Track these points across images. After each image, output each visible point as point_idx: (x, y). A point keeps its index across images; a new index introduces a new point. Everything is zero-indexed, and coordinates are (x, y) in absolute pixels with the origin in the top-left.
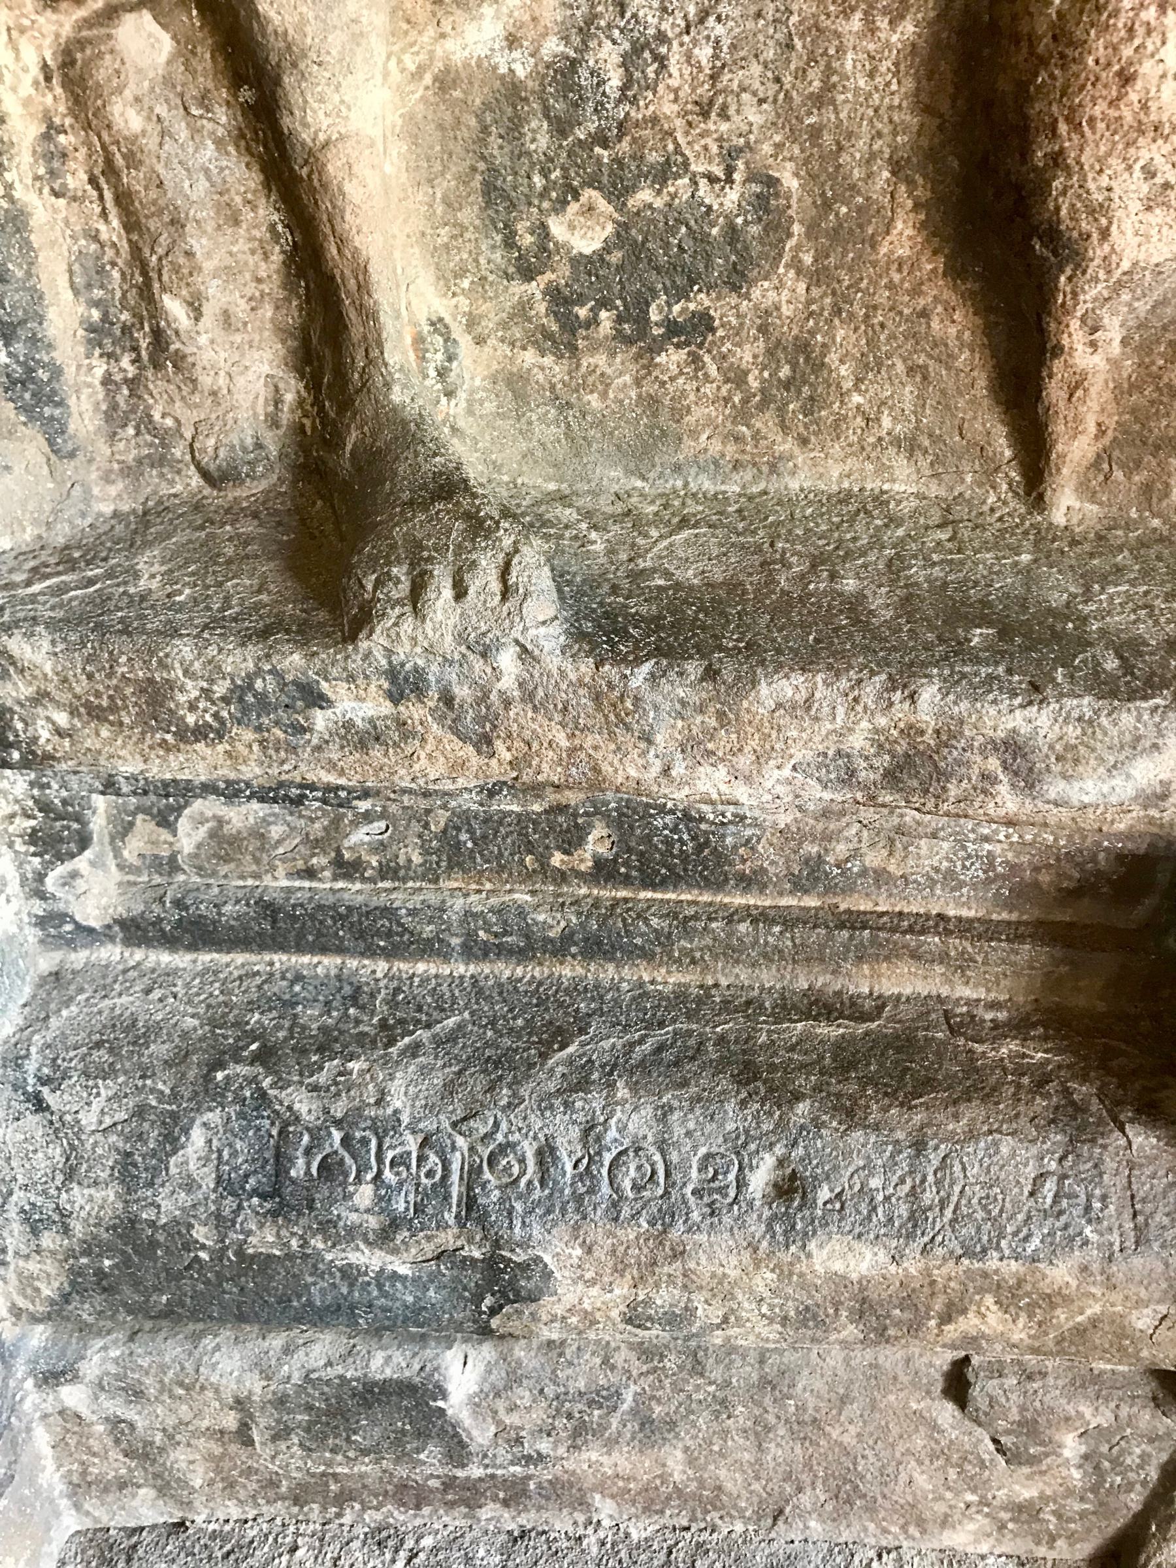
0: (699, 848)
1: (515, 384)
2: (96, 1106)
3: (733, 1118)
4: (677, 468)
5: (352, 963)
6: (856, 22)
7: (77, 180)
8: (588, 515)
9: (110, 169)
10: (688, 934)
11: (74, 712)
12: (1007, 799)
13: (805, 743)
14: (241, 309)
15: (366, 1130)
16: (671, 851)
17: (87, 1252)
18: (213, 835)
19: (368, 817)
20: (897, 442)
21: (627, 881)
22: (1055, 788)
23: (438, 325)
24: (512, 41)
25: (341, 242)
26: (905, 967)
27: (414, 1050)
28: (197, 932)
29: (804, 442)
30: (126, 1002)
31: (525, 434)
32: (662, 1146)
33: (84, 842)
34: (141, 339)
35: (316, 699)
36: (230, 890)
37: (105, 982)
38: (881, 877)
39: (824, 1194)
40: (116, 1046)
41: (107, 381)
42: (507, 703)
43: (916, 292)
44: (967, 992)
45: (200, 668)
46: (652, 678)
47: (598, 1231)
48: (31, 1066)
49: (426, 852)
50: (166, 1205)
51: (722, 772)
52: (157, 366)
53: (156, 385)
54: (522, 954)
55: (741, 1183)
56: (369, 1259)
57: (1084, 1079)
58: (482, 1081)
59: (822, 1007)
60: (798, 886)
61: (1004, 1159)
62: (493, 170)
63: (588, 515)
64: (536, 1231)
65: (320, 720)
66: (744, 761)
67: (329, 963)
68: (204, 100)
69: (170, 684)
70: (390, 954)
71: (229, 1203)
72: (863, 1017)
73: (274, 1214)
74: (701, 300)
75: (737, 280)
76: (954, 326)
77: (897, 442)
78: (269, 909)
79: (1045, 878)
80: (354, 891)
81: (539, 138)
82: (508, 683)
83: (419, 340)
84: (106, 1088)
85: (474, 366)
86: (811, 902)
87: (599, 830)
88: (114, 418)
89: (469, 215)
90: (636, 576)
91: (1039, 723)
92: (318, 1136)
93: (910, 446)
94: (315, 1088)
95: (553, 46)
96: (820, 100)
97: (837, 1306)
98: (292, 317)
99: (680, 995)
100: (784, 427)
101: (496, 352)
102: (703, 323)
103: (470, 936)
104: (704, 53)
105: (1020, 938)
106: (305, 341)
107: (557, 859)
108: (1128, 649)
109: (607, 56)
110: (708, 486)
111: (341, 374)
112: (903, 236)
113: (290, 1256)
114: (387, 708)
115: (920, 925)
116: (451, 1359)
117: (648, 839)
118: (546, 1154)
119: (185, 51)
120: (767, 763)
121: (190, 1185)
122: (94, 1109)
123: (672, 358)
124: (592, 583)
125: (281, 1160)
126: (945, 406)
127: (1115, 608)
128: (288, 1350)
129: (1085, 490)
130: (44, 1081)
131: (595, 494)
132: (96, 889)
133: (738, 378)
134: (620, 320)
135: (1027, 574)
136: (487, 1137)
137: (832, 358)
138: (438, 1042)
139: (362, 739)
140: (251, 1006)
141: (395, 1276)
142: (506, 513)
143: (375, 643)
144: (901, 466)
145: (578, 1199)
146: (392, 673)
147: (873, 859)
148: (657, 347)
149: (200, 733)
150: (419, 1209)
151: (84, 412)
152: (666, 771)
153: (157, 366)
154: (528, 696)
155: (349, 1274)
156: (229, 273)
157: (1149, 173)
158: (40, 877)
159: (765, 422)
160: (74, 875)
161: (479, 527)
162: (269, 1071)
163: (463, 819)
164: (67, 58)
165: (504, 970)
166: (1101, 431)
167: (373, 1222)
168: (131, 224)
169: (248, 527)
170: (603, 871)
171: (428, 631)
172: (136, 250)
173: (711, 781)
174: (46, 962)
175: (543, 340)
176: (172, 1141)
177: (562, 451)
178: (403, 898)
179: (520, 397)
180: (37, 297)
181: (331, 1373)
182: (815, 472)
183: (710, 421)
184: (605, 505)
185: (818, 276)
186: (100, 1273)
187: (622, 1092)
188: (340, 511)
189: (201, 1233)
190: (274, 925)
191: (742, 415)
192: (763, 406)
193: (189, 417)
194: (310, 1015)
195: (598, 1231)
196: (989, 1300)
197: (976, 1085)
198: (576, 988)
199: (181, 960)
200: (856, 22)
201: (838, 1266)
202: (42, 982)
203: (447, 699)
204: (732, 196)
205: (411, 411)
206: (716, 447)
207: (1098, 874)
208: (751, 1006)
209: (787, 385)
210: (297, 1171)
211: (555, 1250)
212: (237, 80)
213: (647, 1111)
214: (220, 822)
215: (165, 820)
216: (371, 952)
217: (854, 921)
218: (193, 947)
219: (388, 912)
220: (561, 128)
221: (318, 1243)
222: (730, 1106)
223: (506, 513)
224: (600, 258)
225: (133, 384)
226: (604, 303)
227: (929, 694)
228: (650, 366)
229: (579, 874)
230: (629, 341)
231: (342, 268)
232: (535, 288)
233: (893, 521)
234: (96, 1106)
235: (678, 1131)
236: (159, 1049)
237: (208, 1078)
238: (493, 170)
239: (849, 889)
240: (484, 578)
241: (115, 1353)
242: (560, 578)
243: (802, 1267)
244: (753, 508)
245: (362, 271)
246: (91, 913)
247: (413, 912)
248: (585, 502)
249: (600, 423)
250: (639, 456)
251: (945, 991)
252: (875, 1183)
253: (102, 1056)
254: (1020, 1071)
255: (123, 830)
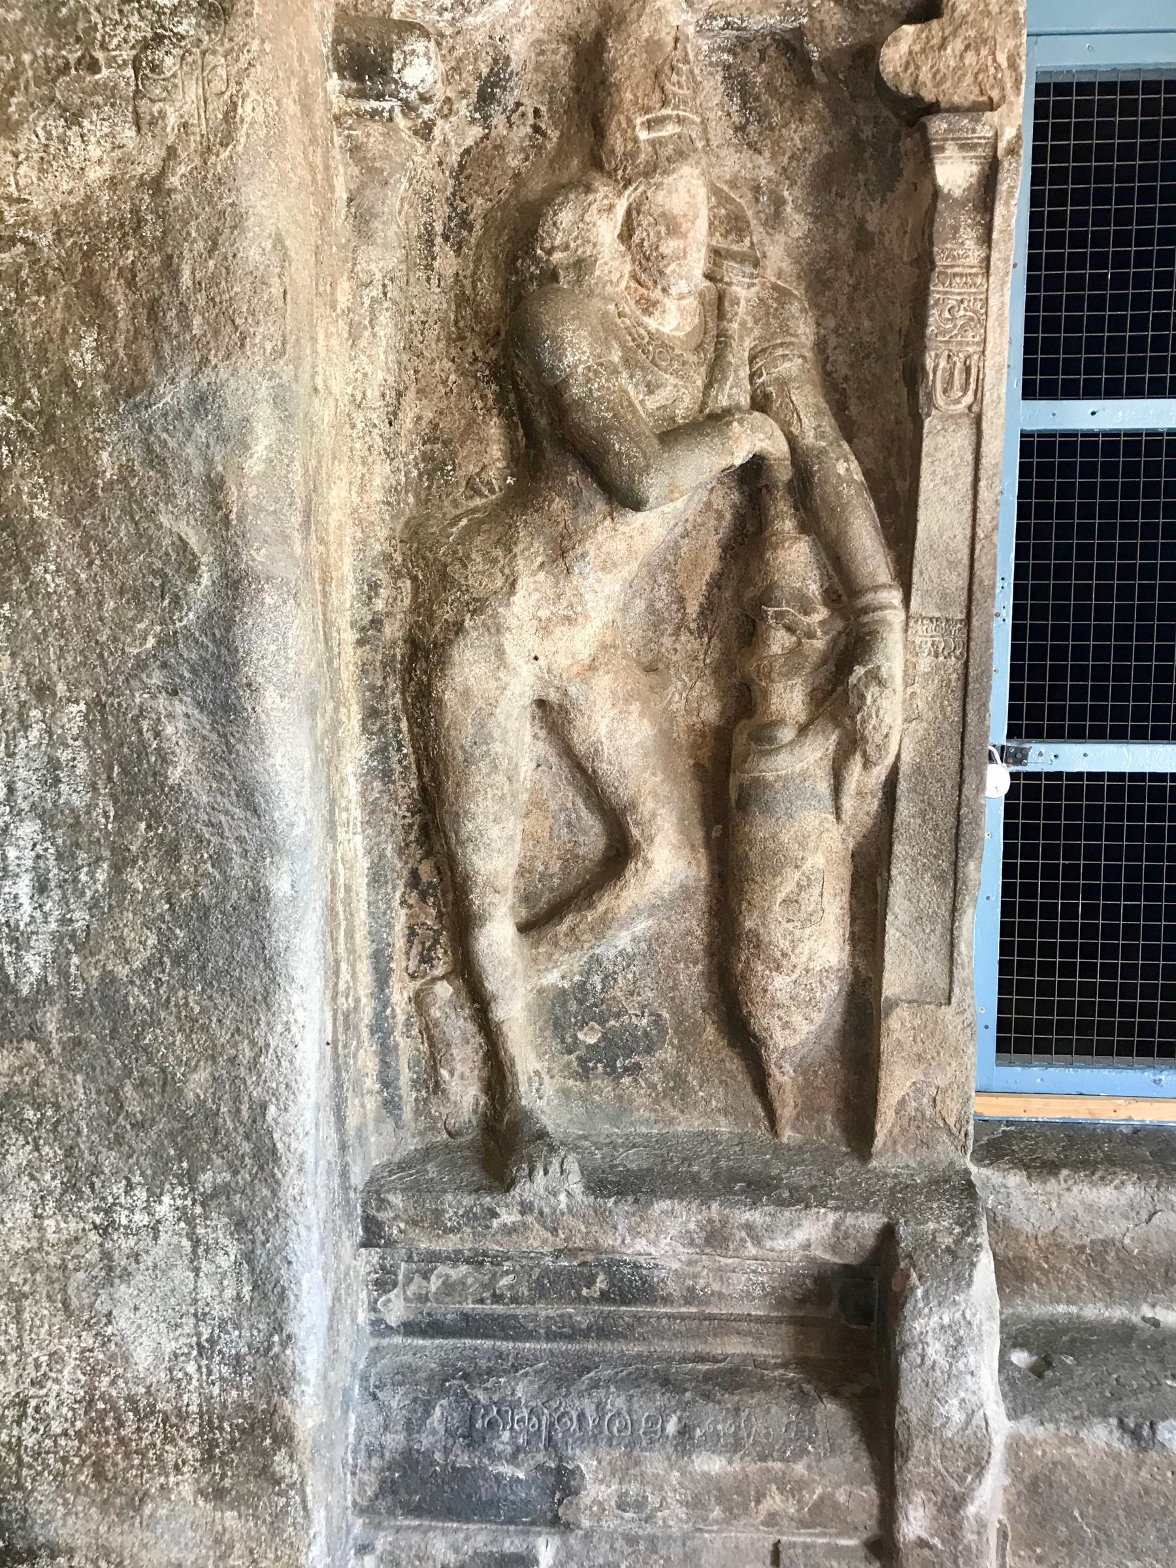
0: (644, 1283)
1: (566, 1093)
2: (398, 1397)
3: (660, 1400)
4: (632, 1123)
5: (498, 1343)
6: (682, 965)
7: (415, 1032)
8: (595, 1144)
9: (427, 1028)
10: (641, 1325)
11: (407, 1223)
12: (752, 1250)
13: (673, 1227)
14: (467, 1072)
15: (507, 1406)
16: (632, 1287)
17: (389, 1469)
18: (444, 1283)
19: (507, 1273)
20: (719, 1111)
21: (614, 1302)
22: (768, 1244)
23: (537, 1073)
24: (563, 978)
25: (506, 1051)
26: (735, 1339)
27: (526, 1374)
28: (433, 1328)
29: (682, 1112)
30: (407, 1358)
31: (570, 1112)
32: (629, 1413)
33: (395, 1285)
34: (431, 1082)
35: (495, 1215)
36: (449, 1311)
37: (397, 1351)
38: (720, 1295)
39: (698, 1432)
40: (404, 1375)
41: (416, 1099)
42: (563, 1214)
43: (718, 1053)
44: (764, 1352)
45: (454, 1204)
46: (615, 1203)
47: (602, 1452)
48: (372, 1381)
49: (530, 1290)
50: (424, 1442)
51: (644, 1241)
52: (435, 1093)
53: (434, 1100)
54: (570, 1338)
55: (663, 1429)
56: (506, 1470)
57: (809, 1382)
58: (554, 1386)
59: (700, 1358)
60: (687, 1303)
61: (772, 1416)
62: (557, 1018)
63: (595, 1144)
64: (578, 1452)
65: (495, 1223)
66: (652, 1236)
67: (488, 1343)
68: (462, 1007)
69: (444, 1211)
70: (515, 1339)
71: (450, 1441)
72: (718, 1362)
73: (468, 1445)
74: (636, 1058)
75: (649, 1051)
76: (734, 1064)
77: (719, 1111)
78: (465, 1316)
79: (788, 1294)
80: (499, 1309)
81: (573, 1006)
82: (563, 1206)
83: (530, 1078)
84: (401, 1390)
85: (549, 1087)
86: (694, 1310)
87: (601, 1278)
88: (417, 1112)
89: (547, 1034)
90: (612, 1167)
91: (755, 1216)
92: (487, 1410)
93: (725, 1112)
94: (486, 1389)
95: (577, 978)
96: (673, 989)
97: (709, 1492)
98: (485, 1074)
99: (639, 1355)
100: (674, 1107)
101: (559, 1080)
102: (637, 1066)
103: (549, 1328)
104: (630, 976)
105: (781, 1322)
106: (489, 1083)
107: (585, 1292)
108: (793, 1189)
109: (596, 980)
110: (644, 1130)
111: (503, 1095)
112: (710, 1032)
113: (474, 1468)
114: (519, 1218)
115: (739, 1319)
116: (541, 1542)
117: (621, 1280)
118: (581, 1416)
119: (457, 992)
120: (660, 1240)
121: (434, 1432)
122: (396, 1400)
123: (626, 1080)
124: (595, 1170)
125: (472, 1421)
126: (736, 1096)
127: (796, 1175)
128: (466, 1539)
129: (794, 1128)
130: (376, 1387)
131: (598, 1135)
132: (396, 1309)
133: (653, 1087)
134: (605, 1067)
135: (767, 1163)
136: (557, 1409)
137: (690, 1078)
138: (536, 1372)
139: (509, 1230)
140: (458, 1359)
141: (518, 1480)
142: (562, 1143)
143: (516, 1192)
144: (723, 1120)
145: (595, 1436)
146: (522, 1204)
147: (716, 1287)
148: (621, 1076)
149: (452, 1230)
150: (528, 1443)
151: (407, 1113)
152: (623, 1242)
153: (435, 1093)
154: (570, 1210)
155: (498, 1478)
156: (463, 1060)
157: (780, 1019)
158: (376, 1301)
159: (666, 1104)
160: (389, 1300)
161: (552, 1149)
162: (467, 1381)
163: (546, 1272)
164: (417, 994)
165: (563, 1346)
166: (796, 1105)
167: (509, 1449)
168: (432, 1045)
169: (467, 1153)
170: (604, 1297)
171: (534, 1187)
172: (432, 1054)
173: (641, 1245)
174: (373, 1343)
175: (576, 1076)
176: (428, 1413)
177: (584, 1117)
178: (520, 1311)
179: (567, 1097)
180: (398, 1071)
181: (485, 1550)
182: (687, 1124)
183: (643, 1104)
184: (602, 1139)
185: (680, 1048)
186: (393, 1481)
187: (612, 1389)
188: (501, 1144)
189: (438, 1456)
190: (469, 1326)
191: (656, 1101)
192: (664, 1097)
193: (444, 1111)
194: (483, 1363)
195: (602, 1452)
196: (774, 1487)
197: (764, 1386)
198: (594, 1353)
199: (427, 1342)
200: (682, 965)
201: (706, 1468)
202: (371, 1351)
203: (541, 1213)
204: (645, 1021)
205: (528, 1107)
206: (647, 1114)
207: (809, 1291)
208: (670, 1360)
209: (673, 1089)
210: (478, 1425)
211: (586, 1462)
212: (474, 1001)
213: (623, 1398)
214: (448, 1276)
215: (426, 1277)
216: (506, 1338)
217: (711, 1318)
218: (432, 1337)
219: (515, 1317)
220: (581, 1002)
221: (486, 1461)
222: (658, 1396)
223: (562, 1143)
224: (596, 1045)
225: (426, 1100)
226: (600, 1061)
227: (715, 1206)
228: (618, 1083)
229: (594, 1299)
230: (609, 1074)
231: (505, 1061)
232: (573, 1057)
233: (719, 1143)
234: (398, 1397)
235: (636, 1406)
236: (422, 1375)
237: (443, 1385)
238: (557, 1018)
239: (708, 1303)
240: (555, 1167)
241: (390, 1539)
242: (582, 1169)
243: (690, 1468)
244: (662, 1139)
245: (512, 1060)
246: (393, 1320)
247: (524, 1317)
248: (594, 1139)
249: (599, 1107)
250: (615, 1120)
251: (754, 1351)
252: (720, 1427)
253: (399, 1377)
254: (782, 1380)
255: (409, 1281)
